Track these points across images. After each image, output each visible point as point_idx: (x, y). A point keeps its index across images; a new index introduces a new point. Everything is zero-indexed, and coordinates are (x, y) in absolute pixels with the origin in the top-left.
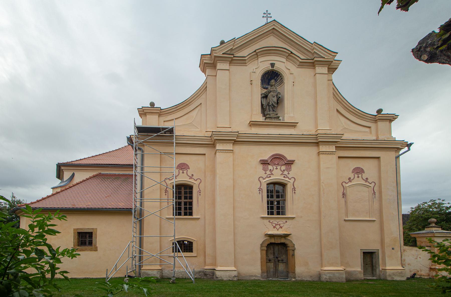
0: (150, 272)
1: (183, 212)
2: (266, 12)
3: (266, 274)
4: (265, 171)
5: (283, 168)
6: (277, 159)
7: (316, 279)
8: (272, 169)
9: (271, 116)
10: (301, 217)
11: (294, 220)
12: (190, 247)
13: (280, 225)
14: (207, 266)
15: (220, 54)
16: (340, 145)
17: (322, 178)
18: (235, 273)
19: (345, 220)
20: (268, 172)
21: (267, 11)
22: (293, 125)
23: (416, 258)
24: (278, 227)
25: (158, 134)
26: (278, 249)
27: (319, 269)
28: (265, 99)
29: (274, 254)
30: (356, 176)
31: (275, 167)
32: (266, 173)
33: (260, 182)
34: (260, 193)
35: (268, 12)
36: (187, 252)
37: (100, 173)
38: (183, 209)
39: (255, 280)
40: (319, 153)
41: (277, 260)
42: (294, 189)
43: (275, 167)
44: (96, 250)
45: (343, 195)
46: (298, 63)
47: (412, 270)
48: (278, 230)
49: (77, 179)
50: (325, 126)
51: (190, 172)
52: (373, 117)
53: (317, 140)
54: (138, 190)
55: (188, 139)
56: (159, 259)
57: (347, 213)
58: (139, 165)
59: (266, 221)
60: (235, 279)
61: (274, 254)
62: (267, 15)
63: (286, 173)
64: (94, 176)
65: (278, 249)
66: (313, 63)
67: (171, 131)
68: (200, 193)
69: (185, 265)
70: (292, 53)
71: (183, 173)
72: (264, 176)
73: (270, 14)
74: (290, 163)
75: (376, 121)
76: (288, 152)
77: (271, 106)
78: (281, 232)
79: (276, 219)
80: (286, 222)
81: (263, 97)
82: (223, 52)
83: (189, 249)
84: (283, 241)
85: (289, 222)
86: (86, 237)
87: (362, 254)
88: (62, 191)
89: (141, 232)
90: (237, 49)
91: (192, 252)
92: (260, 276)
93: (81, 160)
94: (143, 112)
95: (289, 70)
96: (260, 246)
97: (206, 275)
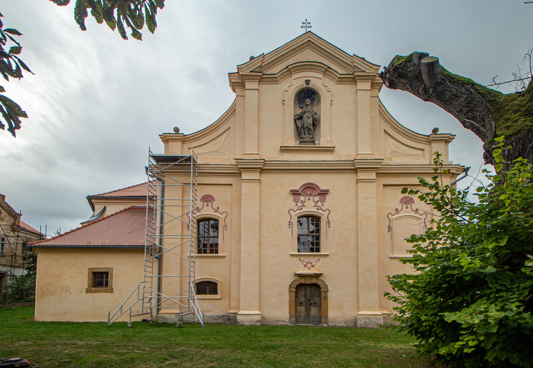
0: (168, 316)
2: (305, 22)
3: (294, 319)
4: (296, 202)
5: (317, 198)
6: (310, 188)
7: (352, 325)
8: (304, 200)
9: (305, 140)
10: (336, 254)
11: (328, 257)
12: (214, 288)
13: (311, 263)
14: (233, 309)
15: (247, 72)
16: (381, 171)
17: (359, 210)
18: (258, 318)
19: (390, 258)
20: (300, 204)
22: (330, 150)
25: (176, 163)
26: (309, 291)
27: (355, 314)
28: (300, 121)
29: (306, 296)
30: (405, 206)
31: (307, 198)
32: (297, 205)
36: (211, 294)
37: (134, 206)
39: (282, 325)
40: (357, 181)
41: (308, 303)
43: (307, 198)
44: (112, 291)
45: (389, 228)
46: (337, 79)
48: (309, 269)
49: (108, 213)
50: (366, 151)
52: (427, 137)
53: (354, 166)
54: (158, 224)
56: (176, 301)
57: (393, 250)
58: (159, 198)
59: (296, 259)
60: (258, 324)
61: (306, 296)
62: (306, 24)
63: (319, 204)
64: (125, 210)
65: (309, 291)
66: (354, 78)
67: (189, 159)
69: (204, 309)
70: (329, 67)
71: (208, 205)
72: (295, 208)
74: (324, 193)
75: (430, 142)
76: (322, 181)
77: (307, 129)
78: (312, 271)
80: (319, 260)
81: (298, 119)
83: (214, 291)
84: (314, 281)
85: (322, 259)
86: (102, 277)
89: (160, 272)
91: (216, 293)
92: (287, 321)
93: (114, 191)
94: (166, 138)
95: (326, 87)
96: (288, 287)
97: (229, 319)
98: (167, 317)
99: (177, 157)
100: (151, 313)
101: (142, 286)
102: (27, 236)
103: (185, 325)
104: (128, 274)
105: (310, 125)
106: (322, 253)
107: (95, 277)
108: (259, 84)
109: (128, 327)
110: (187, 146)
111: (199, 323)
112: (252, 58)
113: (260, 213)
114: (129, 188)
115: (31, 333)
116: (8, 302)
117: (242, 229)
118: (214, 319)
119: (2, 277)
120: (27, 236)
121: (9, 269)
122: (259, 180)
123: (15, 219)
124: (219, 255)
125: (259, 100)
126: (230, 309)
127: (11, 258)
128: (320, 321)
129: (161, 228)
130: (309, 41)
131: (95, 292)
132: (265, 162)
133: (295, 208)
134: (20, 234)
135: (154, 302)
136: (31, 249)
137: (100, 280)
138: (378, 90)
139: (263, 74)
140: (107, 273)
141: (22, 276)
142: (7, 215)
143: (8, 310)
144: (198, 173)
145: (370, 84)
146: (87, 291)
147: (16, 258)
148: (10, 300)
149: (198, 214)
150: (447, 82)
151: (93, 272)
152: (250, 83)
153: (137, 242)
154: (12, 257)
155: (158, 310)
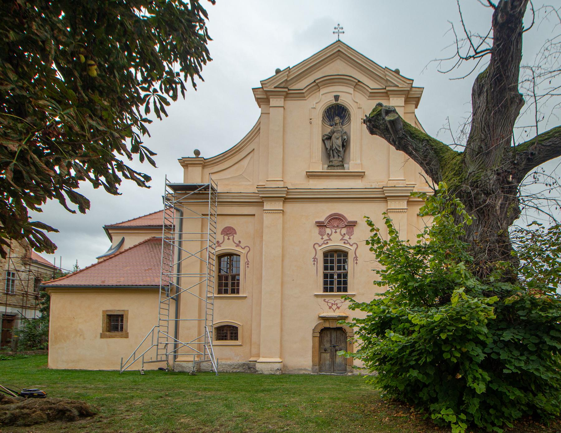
0: (184, 364)
1: (335, 286)
2: (337, 26)
3: (317, 367)
4: (322, 235)
5: (344, 231)
6: (336, 219)
8: (330, 233)
10: (363, 294)
13: (337, 304)
14: (254, 357)
15: (271, 88)
18: (278, 366)
20: (325, 237)
21: (339, 25)
22: (360, 175)
24: (334, 307)
25: (196, 191)
28: (329, 141)
29: (331, 341)
31: (334, 231)
33: (316, 250)
34: (314, 264)
35: (341, 26)
37: (154, 237)
38: (230, 285)
42: (356, 258)
44: (127, 336)
46: (368, 94)
48: (334, 311)
49: (126, 246)
51: (237, 238)
53: (384, 194)
55: (234, 197)
59: (320, 300)
60: (278, 373)
61: (331, 341)
63: (347, 237)
64: (145, 242)
66: (386, 93)
67: (207, 188)
68: (248, 264)
69: (223, 356)
70: (359, 81)
71: (229, 239)
72: (321, 242)
73: (342, 28)
76: (350, 211)
79: (336, 298)
81: (327, 139)
82: (275, 86)
86: (117, 321)
88: (105, 261)
90: (295, 80)
92: (310, 369)
93: (129, 221)
94: (185, 163)
95: (357, 103)
96: (312, 332)
98: (183, 365)
99: (196, 186)
100: (167, 361)
101: (156, 330)
102: (40, 270)
103: (199, 372)
104: (143, 316)
105: (339, 147)
106: (349, 293)
107: (110, 320)
108: (285, 100)
109: (141, 374)
110: (208, 170)
111: (213, 372)
112: (278, 71)
113: (283, 247)
114: (150, 214)
115: (44, 378)
116: (19, 349)
117: (263, 265)
118: (234, 368)
119: (12, 320)
120: (40, 270)
121: (20, 310)
122: (283, 210)
123: (26, 250)
124: (240, 295)
125: (284, 118)
126: (251, 357)
127: (22, 297)
128: (346, 370)
129: (179, 265)
130: (338, 52)
131: (109, 337)
132: (288, 191)
133: (321, 242)
134: (32, 268)
135: (171, 348)
136: (44, 289)
137: (115, 324)
138: (414, 106)
139: (289, 90)
140: (122, 316)
141: (35, 319)
142: (18, 245)
143: (20, 358)
144: (218, 202)
145: (403, 99)
146: (102, 336)
147: (27, 297)
148: (22, 347)
149: (218, 249)
150: (409, 137)
151: (107, 315)
152: (275, 99)
153: (154, 281)
154: (23, 296)
155: (175, 357)
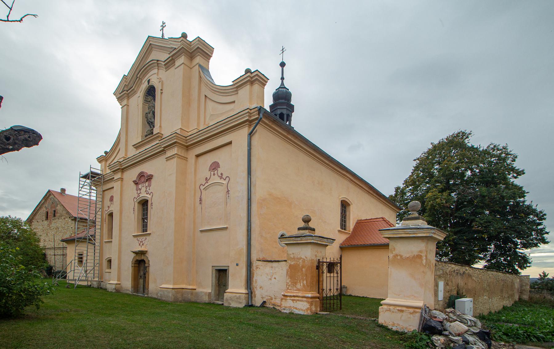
23: (270, 279)
45: (200, 200)
47: (264, 296)
87: (214, 272)
